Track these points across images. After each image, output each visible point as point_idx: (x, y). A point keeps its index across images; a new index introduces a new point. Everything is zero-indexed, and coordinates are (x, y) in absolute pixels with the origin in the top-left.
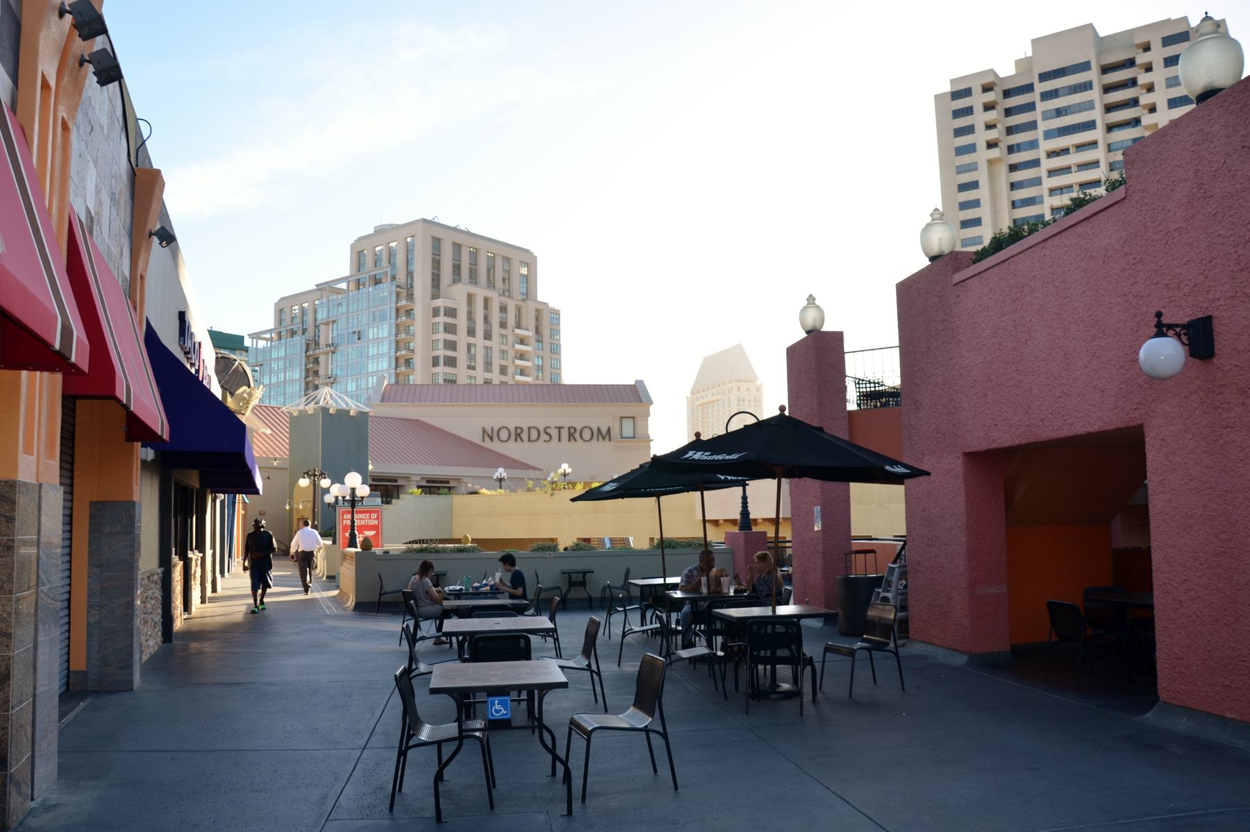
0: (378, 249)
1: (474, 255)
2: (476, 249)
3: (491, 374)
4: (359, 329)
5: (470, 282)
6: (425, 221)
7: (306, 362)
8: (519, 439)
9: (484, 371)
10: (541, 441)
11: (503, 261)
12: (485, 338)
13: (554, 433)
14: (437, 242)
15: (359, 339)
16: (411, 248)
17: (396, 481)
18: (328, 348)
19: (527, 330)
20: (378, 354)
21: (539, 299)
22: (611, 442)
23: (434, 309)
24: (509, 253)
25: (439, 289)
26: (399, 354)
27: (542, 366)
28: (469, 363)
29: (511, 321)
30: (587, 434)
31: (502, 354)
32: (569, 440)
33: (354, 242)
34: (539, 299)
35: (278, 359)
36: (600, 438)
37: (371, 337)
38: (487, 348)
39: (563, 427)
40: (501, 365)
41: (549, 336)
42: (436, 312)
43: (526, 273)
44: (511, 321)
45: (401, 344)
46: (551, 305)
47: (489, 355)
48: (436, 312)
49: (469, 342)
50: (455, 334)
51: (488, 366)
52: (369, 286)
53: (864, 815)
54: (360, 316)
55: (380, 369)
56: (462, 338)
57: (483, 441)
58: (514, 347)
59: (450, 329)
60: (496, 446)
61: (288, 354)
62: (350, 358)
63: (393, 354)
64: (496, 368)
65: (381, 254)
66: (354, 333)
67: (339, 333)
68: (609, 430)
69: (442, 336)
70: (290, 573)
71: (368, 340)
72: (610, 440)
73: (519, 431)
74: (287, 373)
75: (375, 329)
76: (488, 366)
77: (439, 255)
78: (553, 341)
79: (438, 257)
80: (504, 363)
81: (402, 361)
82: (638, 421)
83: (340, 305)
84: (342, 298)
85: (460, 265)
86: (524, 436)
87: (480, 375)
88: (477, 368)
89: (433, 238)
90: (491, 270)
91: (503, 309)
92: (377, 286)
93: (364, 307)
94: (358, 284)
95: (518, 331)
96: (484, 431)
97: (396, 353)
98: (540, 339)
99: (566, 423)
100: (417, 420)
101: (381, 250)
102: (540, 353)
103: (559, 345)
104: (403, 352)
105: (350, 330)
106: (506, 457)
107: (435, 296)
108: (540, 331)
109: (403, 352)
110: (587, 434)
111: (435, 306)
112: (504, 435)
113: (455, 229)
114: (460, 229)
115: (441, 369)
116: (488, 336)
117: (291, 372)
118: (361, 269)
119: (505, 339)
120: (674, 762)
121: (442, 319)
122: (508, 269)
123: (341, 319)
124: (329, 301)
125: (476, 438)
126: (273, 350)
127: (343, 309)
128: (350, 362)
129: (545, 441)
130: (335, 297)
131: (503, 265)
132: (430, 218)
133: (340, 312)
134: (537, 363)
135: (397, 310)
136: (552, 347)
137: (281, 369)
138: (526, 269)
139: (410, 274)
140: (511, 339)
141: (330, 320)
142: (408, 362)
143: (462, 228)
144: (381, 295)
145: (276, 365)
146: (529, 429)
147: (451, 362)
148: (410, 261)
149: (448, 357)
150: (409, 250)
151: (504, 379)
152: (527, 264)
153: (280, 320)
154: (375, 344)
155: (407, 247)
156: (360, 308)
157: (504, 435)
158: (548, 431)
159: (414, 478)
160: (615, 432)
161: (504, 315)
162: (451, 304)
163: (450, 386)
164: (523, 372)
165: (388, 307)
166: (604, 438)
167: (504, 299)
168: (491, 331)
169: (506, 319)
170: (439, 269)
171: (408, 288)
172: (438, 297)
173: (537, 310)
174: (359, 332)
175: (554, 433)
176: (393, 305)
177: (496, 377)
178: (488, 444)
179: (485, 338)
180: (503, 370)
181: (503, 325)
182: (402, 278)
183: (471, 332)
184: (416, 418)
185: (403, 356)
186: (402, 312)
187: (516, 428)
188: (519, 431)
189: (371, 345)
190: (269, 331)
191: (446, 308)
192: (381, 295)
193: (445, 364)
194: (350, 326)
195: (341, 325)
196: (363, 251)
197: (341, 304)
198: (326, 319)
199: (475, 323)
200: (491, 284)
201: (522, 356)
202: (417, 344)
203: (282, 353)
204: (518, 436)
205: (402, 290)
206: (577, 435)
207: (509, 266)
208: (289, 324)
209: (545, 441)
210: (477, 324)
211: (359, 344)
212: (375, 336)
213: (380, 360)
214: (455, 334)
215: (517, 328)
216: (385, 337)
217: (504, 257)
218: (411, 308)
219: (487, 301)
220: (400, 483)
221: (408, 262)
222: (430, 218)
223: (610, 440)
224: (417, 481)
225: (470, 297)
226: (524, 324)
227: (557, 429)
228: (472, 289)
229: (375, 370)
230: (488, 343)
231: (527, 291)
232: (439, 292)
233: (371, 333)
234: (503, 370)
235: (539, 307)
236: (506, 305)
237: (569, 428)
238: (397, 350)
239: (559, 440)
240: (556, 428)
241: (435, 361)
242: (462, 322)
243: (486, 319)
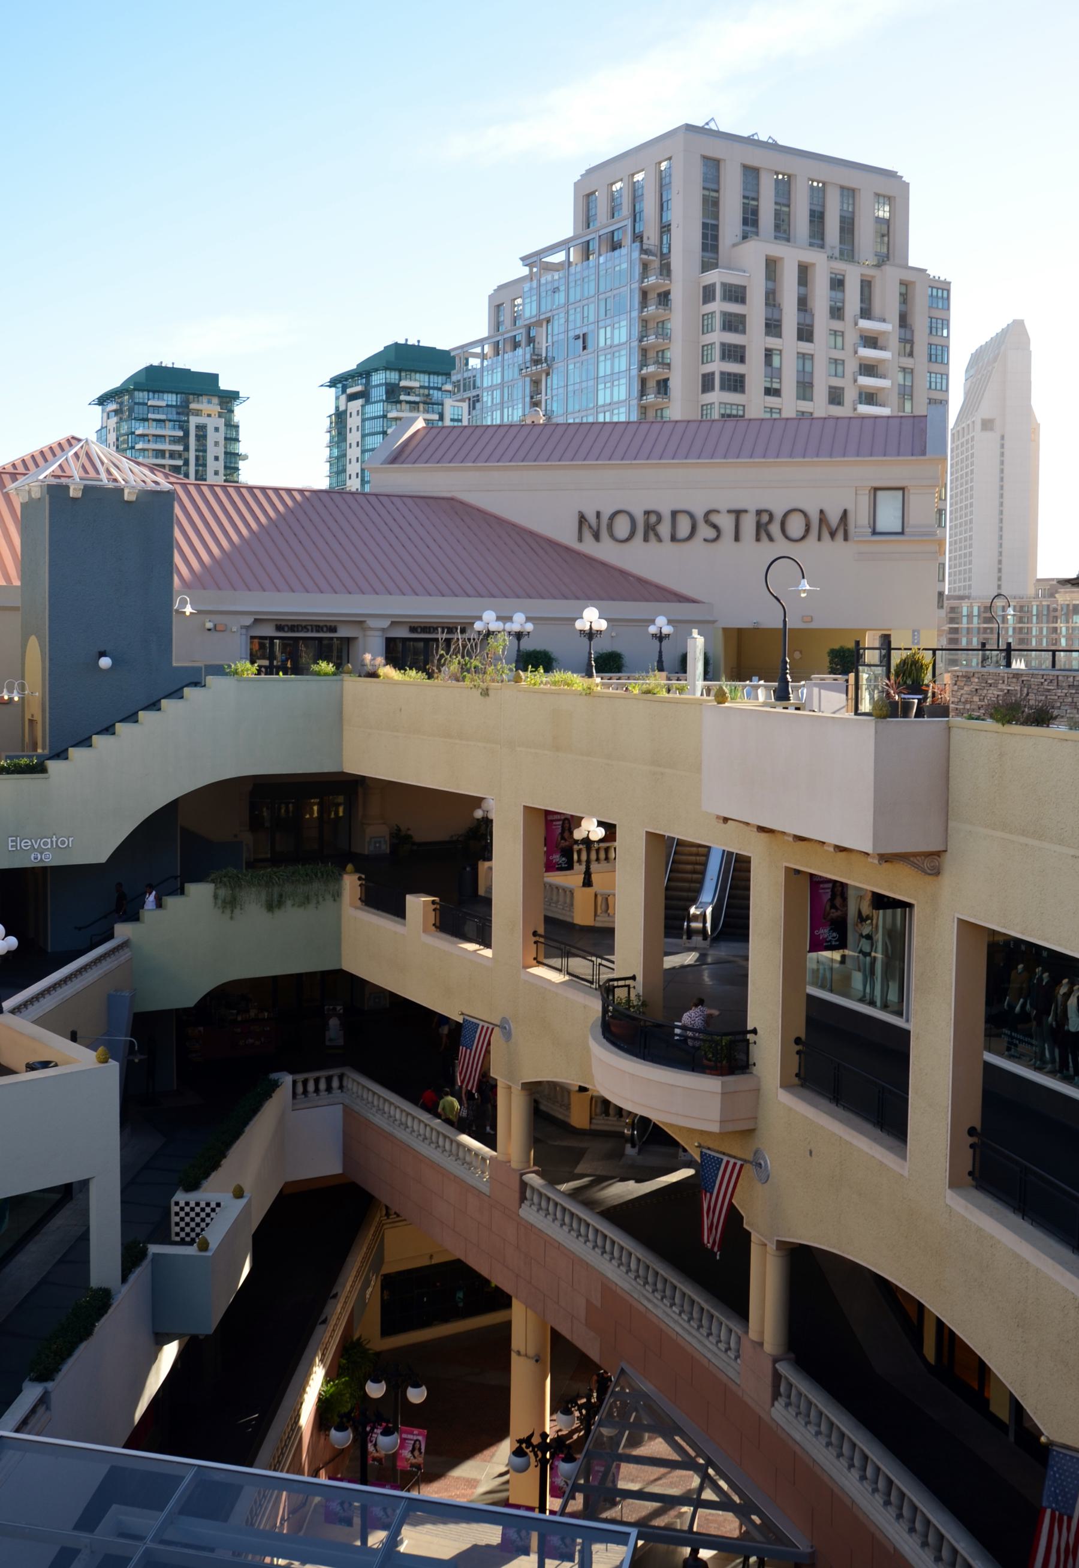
0: (618, 186)
1: (784, 189)
2: (789, 176)
3: (810, 403)
4: (585, 330)
5: (776, 238)
6: (689, 128)
7: (531, 392)
8: (652, 535)
9: (798, 398)
10: (698, 541)
11: (842, 195)
12: (800, 338)
13: (726, 523)
14: (713, 166)
15: (584, 348)
16: (667, 179)
17: (333, 630)
18: (539, 366)
19: (884, 321)
20: (612, 374)
21: (912, 263)
22: (849, 543)
23: (705, 288)
24: (851, 180)
25: (717, 253)
26: (644, 372)
27: (912, 386)
28: (768, 385)
31: (833, 366)
32: (758, 539)
33: (580, 178)
34: (912, 263)
35: (492, 388)
36: (826, 535)
37: (602, 344)
38: (803, 357)
39: (746, 511)
40: (830, 387)
41: (928, 330)
42: (708, 294)
43: (887, 215)
45: (652, 354)
46: (932, 272)
47: (808, 368)
48: (708, 294)
49: (769, 346)
50: (744, 332)
51: (805, 389)
52: (600, 255)
54: (586, 308)
55: (616, 399)
56: (755, 340)
57: (580, 539)
58: (856, 352)
59: (734, 323)
60: (605, 551)
61: (506, 379)
62: (571, 382)
63: (634, 372)
64: (820, 392)
65: (621, 196)
66: (577, 337)
67: (555, 339)
69: (718, 337)
71: (597, 351)
72: (846, 539)
74: (506, 410)
75: (609, 329)
76: (805, 389)
77: (717, 191)
78: (935, 340)
79: (785, 209)
80: (836, 382)
81: (652, 384)
82: (911, 497)
83: (555, 290)
84: (560, 278)
85: (718, 198)
86: (664, 529)
87: (789, 405)
88: (784, 393)
89: (706, 158)
90: (817, 218)
91: (838, 284)
92: (617, 252)
93: (592, 292)
94: (586, 252)
95: (864, 324)
96: (582, 519)
97: (641, 369)
98: (908, 337)
99: (751, 501)
100: (452, 499)
101: (621, 188)
102: (907, 362)
103: (945, 348)
104: (651, 369)
105: (572, 334)
106: (623, 573)
107: (706, 267)
108: (909, 321)
109: (651, 369)
110: (796, 526)
112: (622, 527)
113: (750, 142)
114: (758, 141)
115: (716, 396)
116: (805, 334)
117: (510, 409)
118: (591, 225)
119: (839, 339)
121: (718, 306)
122: (850, 210)
123: (558, 314)
124: (539, 285)
125: (566, 534)
126: (485, 373)
127: (561, 298)
128: (570, 388)
129: (705, 540)
130: (549, 278)
131: (842, 203)
132: (700, 124)
133: (557, 303)
134: (902, 382)
135: (644, 294)
136: (933, 352)
137: (497, 404)
138: (887, 208)
139: (665, 229)
140: (852, 337)
141: (542, 317)
142: (663, 386)
143: (763, 138)
144: (617, 268)
145: (490, 397)
146: (674, 514)
147: (735, 383)
148: (665, 205)
150: (663, 183)
151: (805, 406)
152: (889, 198)
153: (496, 324)
154: (609, 356)
155: (661, 179)
156: (586, 295)
157: (622, 527)
158: (714, 518)
159: (371, 623)
160: (860, 519)
161: (839, 295)
162: (734, 278)
163: (730, 424)
164: (870, 397)
165: (627, 289)
166: (833, 535)
167: (840, 266)
168: (812, 326)
169: (843, 302)
170: (716, 216)
171: (662, 254)
172: (716, 266)
173: (904, 283)
174: (584, 335)
175: (726, 523)
176: (636, 286)
177: (819, 406)
178: (589, 547)
179: (800, 338)
180: (836, 397)
181: (837, 312)
182: (652, 236)
183: (773, 327)
184: (449, 495)
185: (652, 375)
186: (653, 296)
189: (602, 358)
190: (481, 342)
192: (617, 268)
193: (722, 388)
194: (571, 326)
195: (558, 325)
196: (593, 193)
197: (558, 288)
198: (536, 316)
199: (913, 331)
200: (782, 229)
201: (869, 369)
202: (676, 353)
203: (497, 379)
204: (650, 531)
205: (651, 258)
206: (775, 529)
207: (854, 204)
208: (509, 328)
209: (705, 540)
210: (785, 311)
211: (584, 358)
212: (609, 342)
213: (616, 383)
214: (744, 332)
216: (624, 344)
217: (842, 188)
218: (666, 289)
219: (804, 272)
220: (343, 632)
221: (662, 206)
222: (699, 123)
223: (846, 539)
224: (383, 630)
225: (772, 266)
226: (877, 308)
227: (733, 517)
228: (778, 250)
229: (608, 401)
230: (805, 347)
231: (888, 250)
232: (717, 259)
233: (603, 338)
234: (836, 397)
235: (907, 276)
236: (844, 276)
237: (759, 513)
238: (643, 364)
239: (737, 538)
240: (729, 512)
241: (707, 383)
242: (755, 311)
243: (803, 304)
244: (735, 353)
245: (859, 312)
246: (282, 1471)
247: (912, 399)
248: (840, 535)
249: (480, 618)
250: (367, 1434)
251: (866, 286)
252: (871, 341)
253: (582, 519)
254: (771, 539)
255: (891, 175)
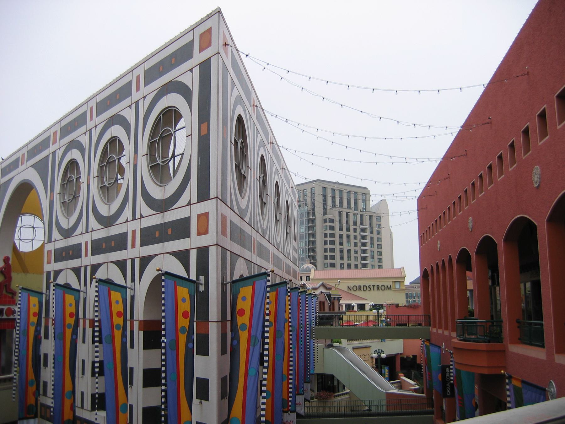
8: (360, 290)
14: (325, 189)
19: (366, 226)
24: (356, 190)
29: (359, 222)
30: (383, 288)
32: (377, 290)
36: (388, 289)
39: (375, 286)
44: (359, 222)
48: (325, 221)
53: (24, 170)
56: (337, 232)
59: (332, 228)
68: (391, 286)
69: (328, 232)
70: (485, 320)
73: (360, 287)
86: (362, 289)
95: (362, 226)
96: (348, 287)
110: (383, 288)
111: (326, 255)
116: (348, 230)
120: (213, 246)
121: (328, 224)
139: (313, 204)
146: (363, 286)
149: (331, 241)
157: (355, 289)
158: (370, 287)
166: (389, 289)
175: (372, 287)
181: (355, 224)
183: (341, 229)
187: (359, 286)
188: (360, 287)
191: (330, 241)
206: (380, 288)
213: (301, 242)
215: (361, 225)
225: (340, 213)
237: (377, 286)
238: (308, 231)
239: (374, 290)
240: (373, 286)
242: (337, 225)
244: (332, 235)
245: (361, 259)
246: (336, 393)
247: (373, 245)
248: (390, 289)
249: (352, 304)
250: (419, 339)
251: (362, 216)
252: (363, 230)
253: (348, 287)
254: (379, 290)
255: (365, 188)
